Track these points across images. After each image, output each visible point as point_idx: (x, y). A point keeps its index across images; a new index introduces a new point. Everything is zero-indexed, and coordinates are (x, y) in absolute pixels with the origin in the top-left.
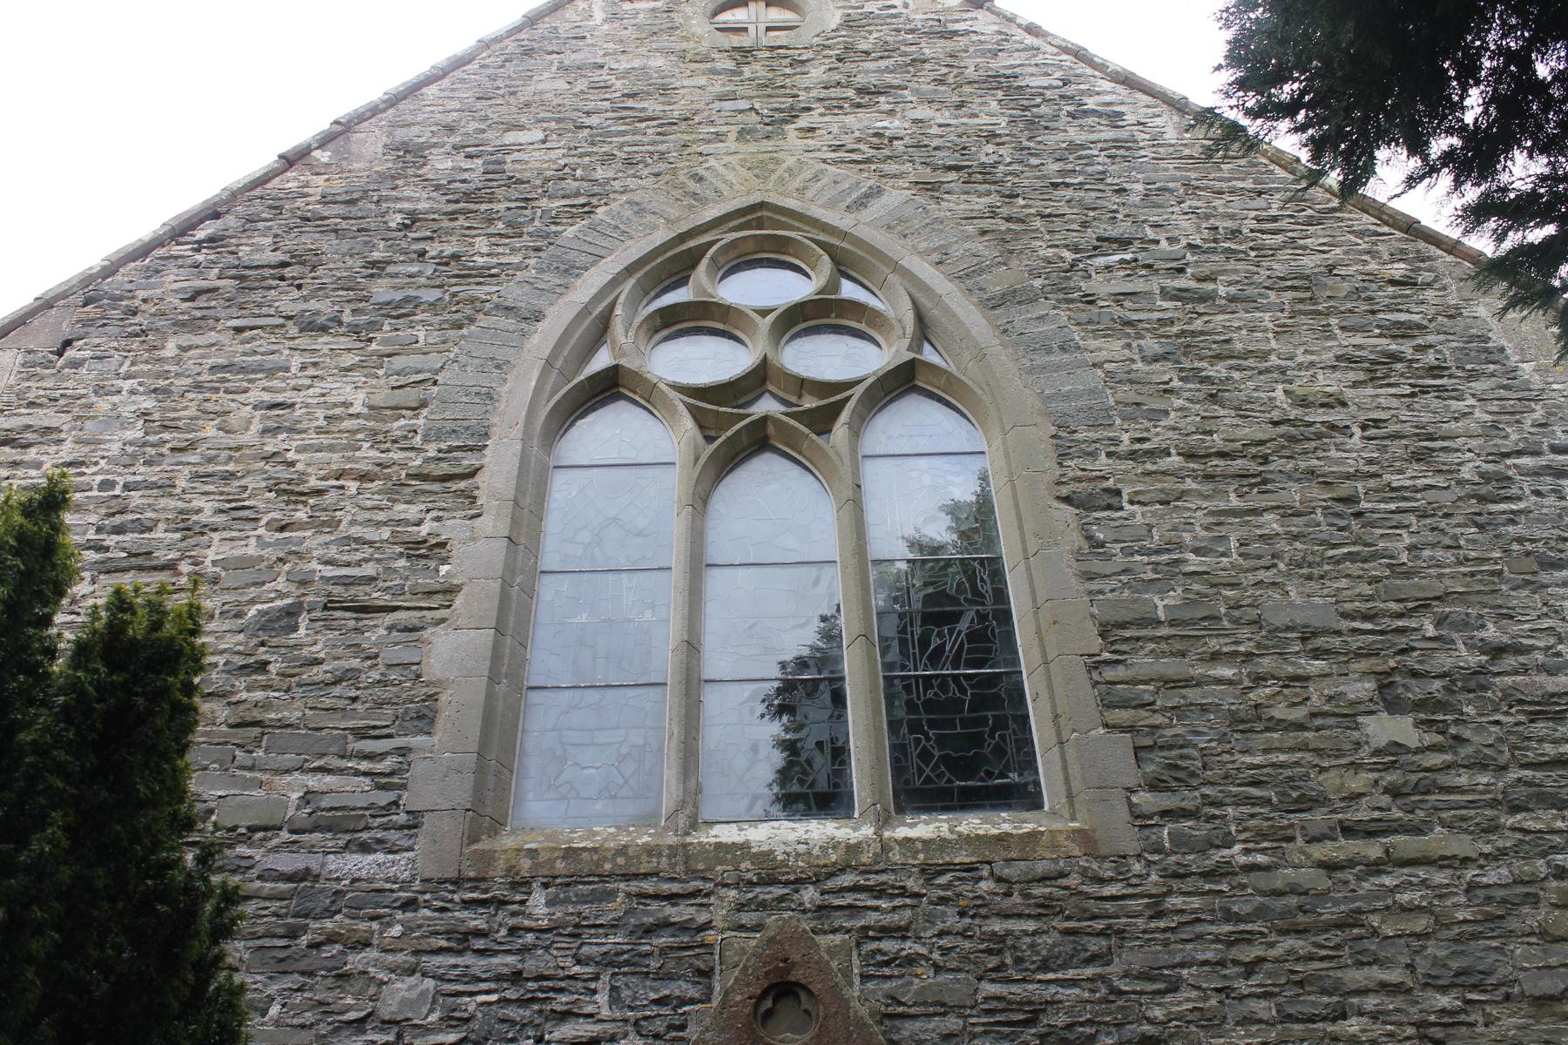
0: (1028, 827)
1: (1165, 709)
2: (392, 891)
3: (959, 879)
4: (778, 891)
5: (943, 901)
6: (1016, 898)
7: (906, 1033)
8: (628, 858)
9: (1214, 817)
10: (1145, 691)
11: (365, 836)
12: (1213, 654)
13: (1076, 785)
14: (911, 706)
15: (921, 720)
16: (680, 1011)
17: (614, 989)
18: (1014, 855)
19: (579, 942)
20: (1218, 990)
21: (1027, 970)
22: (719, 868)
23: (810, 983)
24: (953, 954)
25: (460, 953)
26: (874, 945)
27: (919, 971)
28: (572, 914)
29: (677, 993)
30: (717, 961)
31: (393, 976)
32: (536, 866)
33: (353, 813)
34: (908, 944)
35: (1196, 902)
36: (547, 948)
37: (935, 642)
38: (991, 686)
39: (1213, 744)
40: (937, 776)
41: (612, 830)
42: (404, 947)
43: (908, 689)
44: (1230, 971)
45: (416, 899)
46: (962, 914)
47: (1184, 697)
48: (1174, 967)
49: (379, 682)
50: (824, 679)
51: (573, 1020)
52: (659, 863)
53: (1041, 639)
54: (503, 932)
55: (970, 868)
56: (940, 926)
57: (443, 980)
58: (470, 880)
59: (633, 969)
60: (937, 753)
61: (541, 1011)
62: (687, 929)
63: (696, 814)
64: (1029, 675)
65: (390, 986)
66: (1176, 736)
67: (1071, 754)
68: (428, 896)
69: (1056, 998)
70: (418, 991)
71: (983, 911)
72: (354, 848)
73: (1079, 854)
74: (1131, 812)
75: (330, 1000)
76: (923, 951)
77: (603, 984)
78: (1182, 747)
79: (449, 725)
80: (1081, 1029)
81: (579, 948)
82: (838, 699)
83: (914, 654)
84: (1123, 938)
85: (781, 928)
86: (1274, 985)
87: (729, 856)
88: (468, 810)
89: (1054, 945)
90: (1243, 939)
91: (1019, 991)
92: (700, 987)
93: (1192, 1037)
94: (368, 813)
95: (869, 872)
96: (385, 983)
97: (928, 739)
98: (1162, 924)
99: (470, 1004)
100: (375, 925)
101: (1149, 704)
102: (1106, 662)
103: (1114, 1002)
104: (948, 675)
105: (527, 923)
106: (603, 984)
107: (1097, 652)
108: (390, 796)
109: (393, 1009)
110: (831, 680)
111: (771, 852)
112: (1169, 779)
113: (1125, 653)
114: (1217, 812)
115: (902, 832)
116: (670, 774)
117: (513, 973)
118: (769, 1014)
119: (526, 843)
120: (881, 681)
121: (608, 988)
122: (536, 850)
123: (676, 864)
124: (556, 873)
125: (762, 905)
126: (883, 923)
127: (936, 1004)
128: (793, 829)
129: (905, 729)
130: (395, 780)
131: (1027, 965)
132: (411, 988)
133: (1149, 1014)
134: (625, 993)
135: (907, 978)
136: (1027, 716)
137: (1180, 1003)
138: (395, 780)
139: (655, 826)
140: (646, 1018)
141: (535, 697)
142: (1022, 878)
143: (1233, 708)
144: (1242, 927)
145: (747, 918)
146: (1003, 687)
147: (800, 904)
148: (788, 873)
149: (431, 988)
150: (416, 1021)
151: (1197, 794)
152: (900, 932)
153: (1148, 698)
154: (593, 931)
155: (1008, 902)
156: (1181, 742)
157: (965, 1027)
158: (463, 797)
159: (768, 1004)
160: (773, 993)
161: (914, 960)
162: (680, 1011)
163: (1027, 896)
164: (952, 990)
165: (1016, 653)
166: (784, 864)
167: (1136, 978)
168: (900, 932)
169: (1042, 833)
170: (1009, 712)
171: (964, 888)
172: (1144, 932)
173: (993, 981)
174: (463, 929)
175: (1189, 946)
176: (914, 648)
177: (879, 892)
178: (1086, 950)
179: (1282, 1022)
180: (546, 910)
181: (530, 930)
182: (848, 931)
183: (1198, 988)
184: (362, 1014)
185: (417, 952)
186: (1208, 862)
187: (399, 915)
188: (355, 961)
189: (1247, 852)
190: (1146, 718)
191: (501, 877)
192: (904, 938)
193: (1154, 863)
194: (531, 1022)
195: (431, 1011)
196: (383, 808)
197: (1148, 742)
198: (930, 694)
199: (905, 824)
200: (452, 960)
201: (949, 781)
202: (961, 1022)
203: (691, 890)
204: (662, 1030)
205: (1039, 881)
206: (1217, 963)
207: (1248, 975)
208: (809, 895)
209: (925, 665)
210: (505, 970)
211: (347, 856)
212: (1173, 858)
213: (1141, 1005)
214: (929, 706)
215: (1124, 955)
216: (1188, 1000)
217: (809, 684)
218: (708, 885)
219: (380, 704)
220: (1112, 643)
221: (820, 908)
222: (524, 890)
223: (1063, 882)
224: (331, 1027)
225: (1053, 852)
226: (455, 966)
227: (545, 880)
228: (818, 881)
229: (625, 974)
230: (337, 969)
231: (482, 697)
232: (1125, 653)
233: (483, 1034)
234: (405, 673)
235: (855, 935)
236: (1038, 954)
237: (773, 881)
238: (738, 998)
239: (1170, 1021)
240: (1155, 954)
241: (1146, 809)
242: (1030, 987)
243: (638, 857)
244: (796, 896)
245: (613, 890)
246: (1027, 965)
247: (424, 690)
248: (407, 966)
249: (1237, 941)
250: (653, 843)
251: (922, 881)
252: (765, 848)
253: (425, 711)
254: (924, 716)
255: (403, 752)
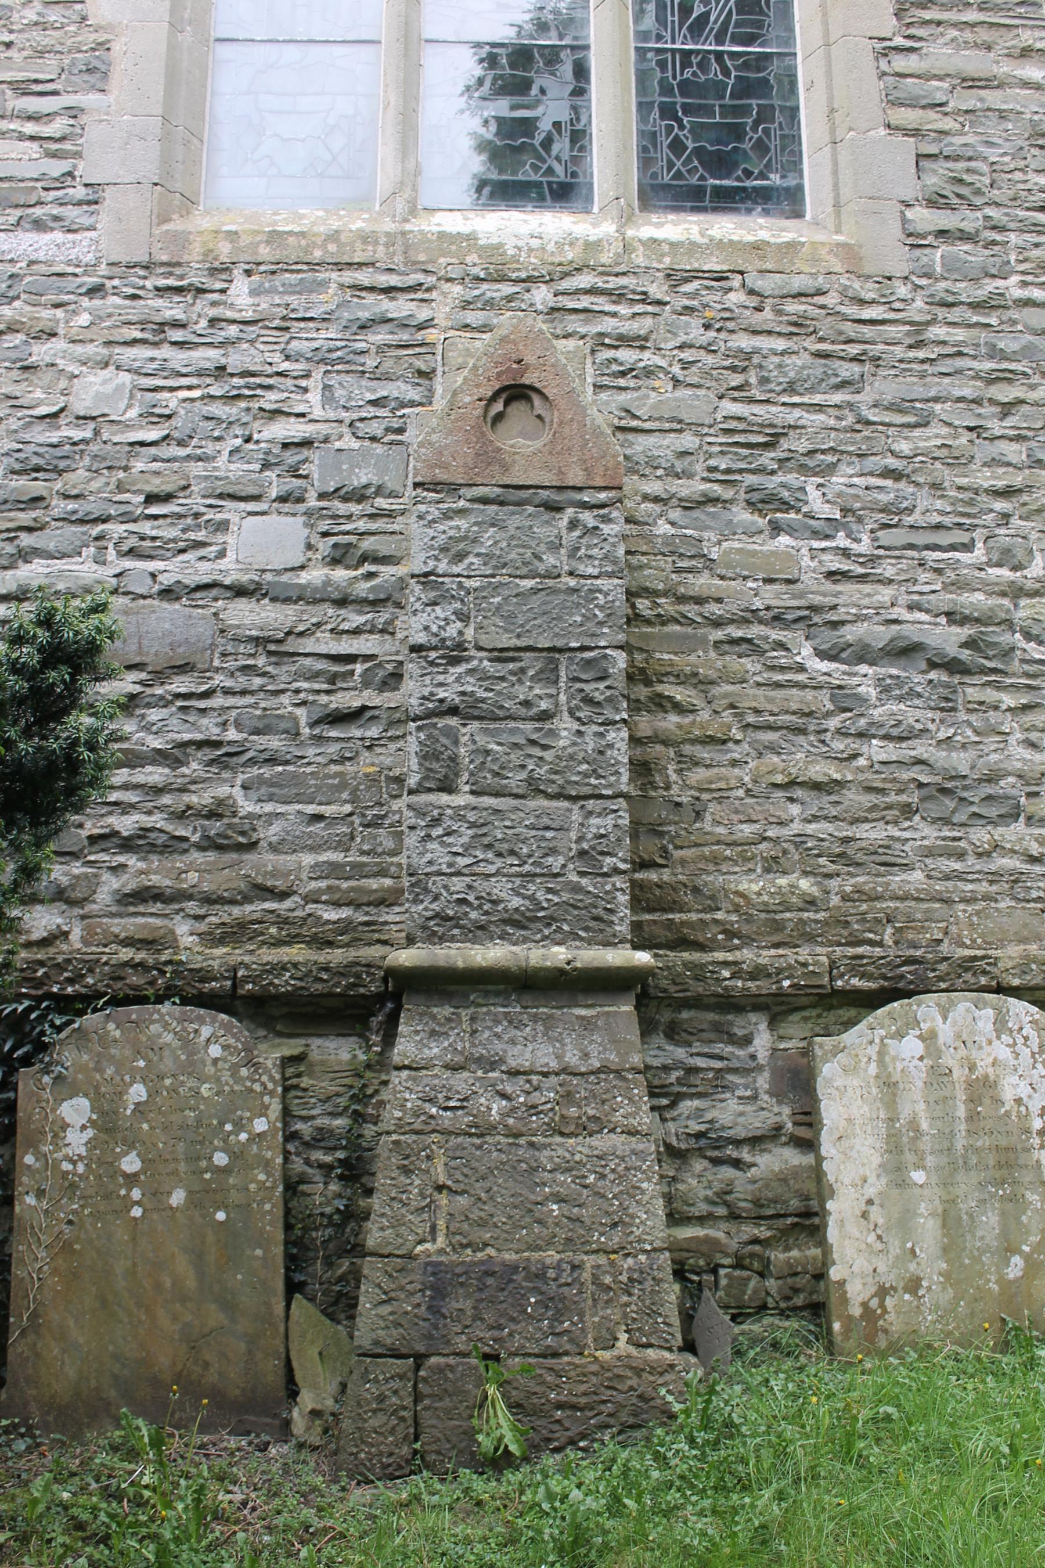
0: (787, 237)
1: (959, 112)
2: (75, 275)
3: (707, 288)
4: (507, 289)
5: (688, 310)
6: (768, 313)
7: (640, 449)
8: (340, 245)
9: (994, 243)
10: (938, 88)
11: (38, 212)
12: (1023, 49)
13: (846, 193)
14: (666, 89)
15: (675, 103)
16: (398, 413)
17: (326, 387)
18: (769, 266)
19: (288, 336)
20: (970, 429)
21: (771, 391)
22: (442, 261)
23: (545, 387)
24: (694, 369)
25: (155, 344)
26: (611, 354)
27: (657, 384)
28: (278, 305)
29: (395, 394)
30: (440, 362)
31: (84, 368)
32: (237, 250)
33: (21, 185)
34: (647, 355)
35: (960, 334)
36: (252, 342)
37: (698, 10)
38: (759, 70)
39: (1007, 159)
40: (689, 171)
41: (321, 213)
42: (94, 337)
43: (662, 65)
44: (986, 410)
45: (103, 285)
46: (707, 327)
47: (982, 100)
48: (928, 401)
49: (36, 24)
50: (565, 47)
51: (283, 419)
52: (375, 252)
53: (825, 14)
54: (203, 323)
55: (720, 277)
56: (682, 338)
57: (140, 374)
58: (163, 264)
59: (347, 367)
60: (690, 145)
61: (248, 409)
62: (406, 325)
63: (416, 199)
64: (804, 59)
65: (81, 379)
66: (965, 145)
67: (844, 156)
68: (116, 282)
69: (800, 423)
70: (113, 385)
71: (730, 325)
72: (28, 226)
73: (841, 271)
74: (904, 229)
75: (18, 394)
76: (663, 363)
77: (315, 383)
78: (970, 159)
79: (126, 82)
80: (822, 457)
81: (288, 343)
82: (581, 71)
83: (673, 22)
84: (878, 366)
85: (515, 327)
86: (1029, 429)
87: (454, 248)
88: (156, 184)
89: (803, 368)
90: (1005, 379)
91: (762, 413)
92: (420, 389)
93: (936, 474)
94: (39, 185)
95: (609, 274)
96: (76, 377)
97: (682, 127)
98: (921, 354)
99: (172, 401)
100: (59, 313)
101: (940, 105)
102: (898, 49)
103: (860, 431)
104: (709, 52)
105: (229, 314)
106: (315, 383)
107: (889, 35)
108: (64, 166)
109: (87, 404)
110: (573, 48)
111: (501, 245)
112: (951, 195)
113: (921, 39)
114: (998, 238)
115: (647, 232)
116: (386, 152)
117: (217, 368)
118: (499, 417)
119: (223, 224)
120: (632, 53)
121: (321, 386)
122: (236, 233)
123: (394, 254)
124: (260, 260)
125: (489, 304)
126: (621, 330)
127: (672, 420)
128: (525, 221)
129: (656, 113)
130: (67, 146)
131: (772, 386)
132: (105, 382)
133: (895, 447)
134: (339, 393)
135: (643, 391)
136: (797, 108)
137: (929, 438)
138: (67, 146)
139: (369, 211)
140: (362, 420)
141: (224, 51)
142: (776, 292)
143: (1036, 117)
144: (1005, 365)
145: (472, 317)
146: (775, 65)
147: (531, 305)
148: (518, 269)
149: (128, 383)
150: (112, 418)
151: (979, 214)
152: (639, 342)
153: (940, 97)
154: (302, 325)
155: (758, 317)
156: (970, 154)
157: (700, 447)
158: (149, 169)
159: (498, 407)
160: (504, 396)
161: (651, 372)
162: (398, 413)
163: (779, 312)
164: (691, 406)
165: (791, 29)
166: (515, 259)
167: (887, 409)
168: (639, 342)
169: (803, 244)
170: (777, 102)
171: (709, 298)
172: (901, 361)
173: (735, 400)
174: (158, 320)
175: (947, 380)
176: (673, 15)
177: (618, 296)
178: (837, 375)
179: (1030, 467)
180: (250, 301)
181: (234, 322)
182: (583, 337)
183: (950, 425)
184: (54, 409)
185: (109, 343)
186: (979, 292)
187: (85, 302)
188: (41, 352)
189: (1024, 284)
190: (934, 120)
191: (198, 262)
192: (643, 348)
193: (922, 287)
194: (238, 420)
195: (129, 406)
196: (56, 179)
197: (933, 149)
198: (688, 74)
199: (650, 223)
200: (148, 352)
201: (702, 178)
202: (697, 440)
203: (411, 283)
204: (379, 433)
205: (794, 297)
206: (973, 401)
207: (1004, 415)
208: (542, 296)
209: (685, 37)
210: (207, 365)
211: (20, 234)
212: (943, 285)
213: (888, 437)
214: (685, 87)
215: (877, 384)
216: (937, 436)
217: (547, 51)
218: (429, 279)
219: (41, 53)
220: (909, 25)
221: (553, 310)
222: (224, 277)
223: (820, 300)
224: (22, 422)
225: (812, 267)
226: (152, 359)
227: (247, 267)
228: (552, 280)
229: (338, 372)
230: (21, 360)
231: (163, 48)
232: (921, 39)
233: (188, 432)
234: (67, 13)
235: (590, 343)
236: (786, 375)
237: (503, 279)
238: (468, 399)
239: (916, 456)
240: (911, 387)
241: (921, 228)
242: (774, 409)
243: (352, 244)
244: (527, 296)
245: (323, 280)
246: (772, 386)
247: (93, 36)
248: (99, 358)
249: (998, 379)
250: (368, 230)
251: (666, 288)
252: (495, 240)
253: (96, 63)
254: (679, 100)
255: (73, 112)
